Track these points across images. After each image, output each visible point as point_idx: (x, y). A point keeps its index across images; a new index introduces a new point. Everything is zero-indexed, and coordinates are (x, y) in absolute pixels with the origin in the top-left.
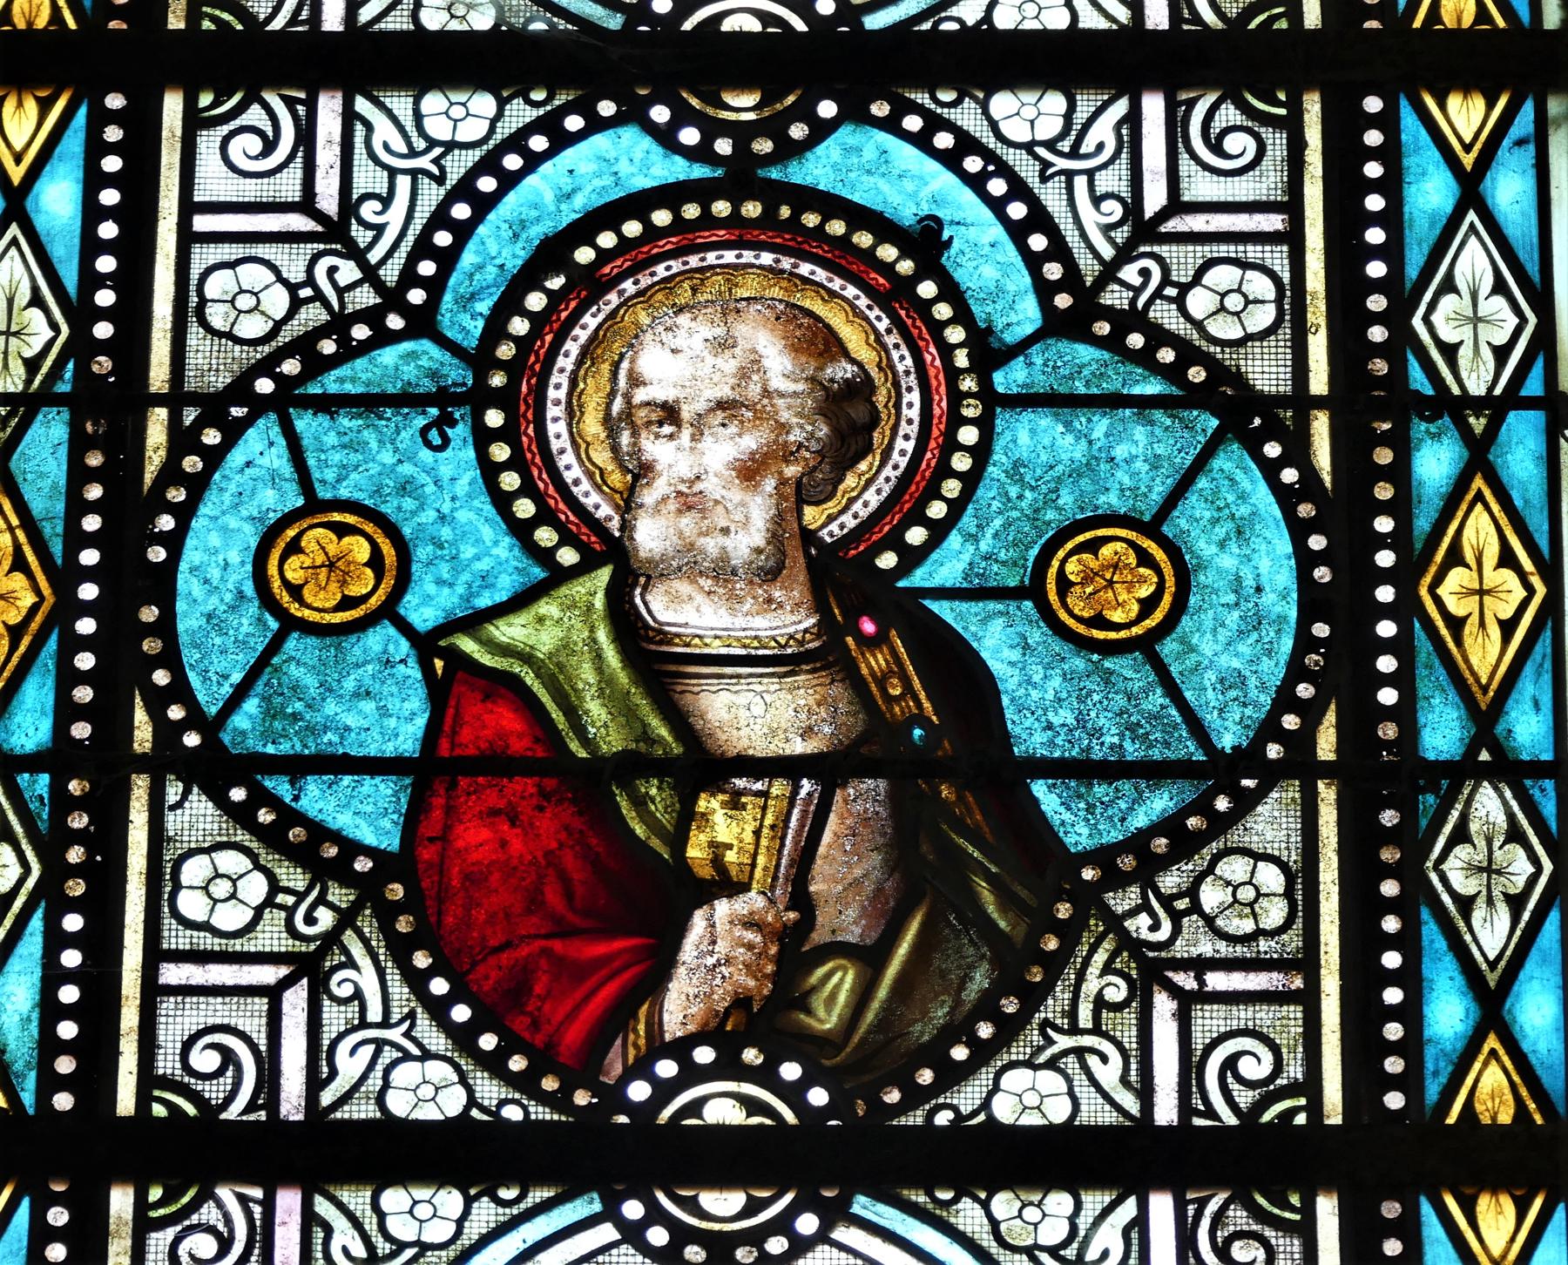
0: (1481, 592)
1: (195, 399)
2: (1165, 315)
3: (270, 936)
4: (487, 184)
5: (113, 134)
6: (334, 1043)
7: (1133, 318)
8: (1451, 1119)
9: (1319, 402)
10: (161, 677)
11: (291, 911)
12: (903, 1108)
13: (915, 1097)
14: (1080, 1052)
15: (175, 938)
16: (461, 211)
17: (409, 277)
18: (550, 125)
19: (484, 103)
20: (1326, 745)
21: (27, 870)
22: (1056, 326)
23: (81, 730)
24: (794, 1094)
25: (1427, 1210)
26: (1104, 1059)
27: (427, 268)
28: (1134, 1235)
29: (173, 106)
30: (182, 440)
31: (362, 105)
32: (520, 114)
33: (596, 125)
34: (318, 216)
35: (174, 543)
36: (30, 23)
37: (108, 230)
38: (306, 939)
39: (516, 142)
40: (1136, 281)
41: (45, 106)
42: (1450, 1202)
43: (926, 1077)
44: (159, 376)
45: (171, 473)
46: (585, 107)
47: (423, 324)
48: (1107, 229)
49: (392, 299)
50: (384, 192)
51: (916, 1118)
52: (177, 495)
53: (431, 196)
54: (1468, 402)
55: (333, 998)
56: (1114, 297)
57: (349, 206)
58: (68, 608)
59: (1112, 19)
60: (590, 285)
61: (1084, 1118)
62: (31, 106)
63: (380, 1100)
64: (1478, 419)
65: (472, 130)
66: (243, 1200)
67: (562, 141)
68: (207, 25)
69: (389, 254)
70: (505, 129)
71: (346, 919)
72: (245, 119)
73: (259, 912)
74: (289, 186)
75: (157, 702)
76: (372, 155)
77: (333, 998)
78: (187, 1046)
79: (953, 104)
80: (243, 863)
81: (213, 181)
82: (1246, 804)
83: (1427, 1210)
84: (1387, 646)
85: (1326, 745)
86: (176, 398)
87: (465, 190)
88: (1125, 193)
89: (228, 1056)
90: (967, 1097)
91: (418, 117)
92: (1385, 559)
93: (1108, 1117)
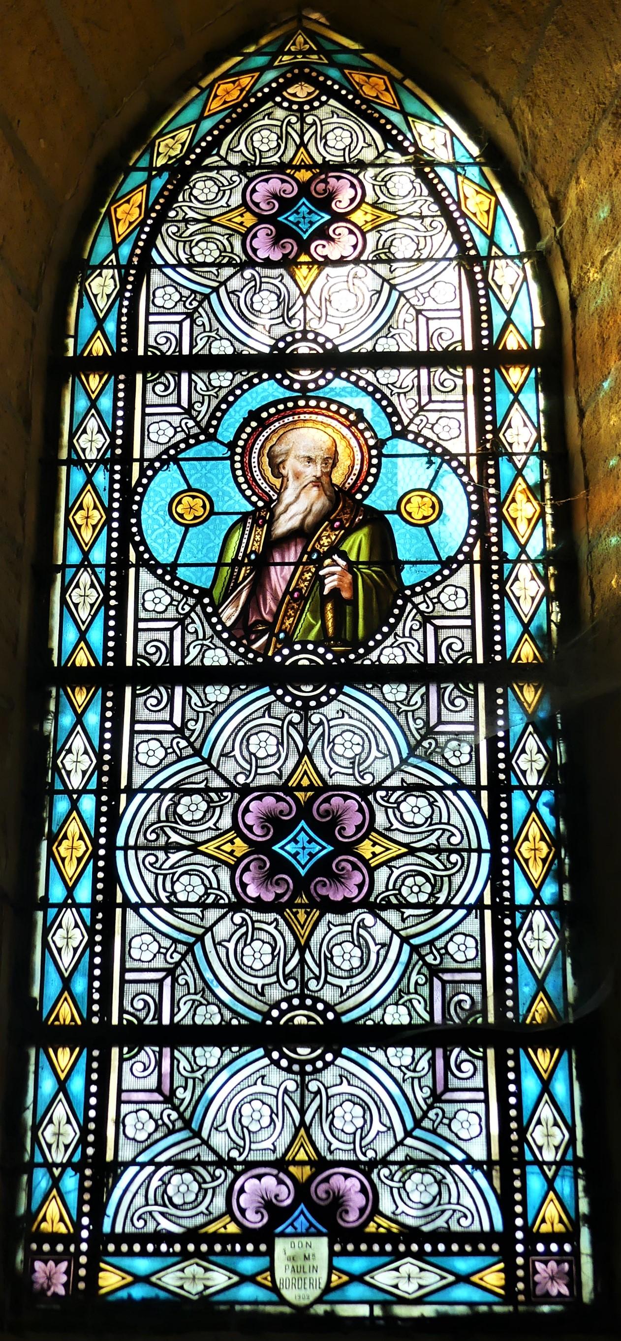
0: (535, 850)
1: (147, 460)
3: (159, 963)
4: (231, 399)
5: (121, 386)
6: (188, 646)
7: (418, 435)
8: (500, 348)
9: (484, 788)
10: (137, 538)
11: (177, 606)
12: (356, 659)
13: (359, 657)
14: (406, 643)
15: (142, 615)
16: (224, 406)
17: (209, 425)
19: (229, 375)
21: (99, 595)
22: (396, 435)
23: (100, 898)
25: (522, 1052)
26: (413, 645)
27: (214, 423)
28: (425, 698)
29: (139, 378)
31: (194, 377)
32: (239, 379)
33: (262, 381)
34: (182, 408)
35: (140, 504)
36: (81, 689)
37: (111, 654)
38: (181, 614)
39: (239, 386)
40: (427, 746)
41: (101, 378)
42: (530, 1050)
43: (361, 651)
44: (136, 455)
45: (139, 483)
46: (259, 376)
47: (212, 438)
49: (204, 431)
50: (195, 718)
51: (359, 662)
52: (140, 490)
53: (215, 403)
54: (529, 787)
55: (188, 632)
56: (412, 428)
57: (184, 723)
58: (109, 520)
59: (418, 660)
60: (263, 424)
61: (408, 662)
62: (97, 377)
63: (202, 661)
64: (559, 1293)
65: (226, 383)
66: (154, 1052)
67: (252, 385)
68: (150, 354)
69: (197, 738)
70: (235, 383)
71: (193, 608)
72: (153, 694)
74: (173, 399)
75: (136, 546)
76: (197, 392)
77: (188, 632)
79: (372, 688)
80: (162, 593)
81: (151, 398)
82: (453, 572)
83: (522, 1052)
84: (506, 867)
86: (142, 460)
87: (224, 400)
88: (424, 717)
89: (158, 648)
90: (374, 656)
91: (210, 380)
92: (495, 558)
93: (414, 662)
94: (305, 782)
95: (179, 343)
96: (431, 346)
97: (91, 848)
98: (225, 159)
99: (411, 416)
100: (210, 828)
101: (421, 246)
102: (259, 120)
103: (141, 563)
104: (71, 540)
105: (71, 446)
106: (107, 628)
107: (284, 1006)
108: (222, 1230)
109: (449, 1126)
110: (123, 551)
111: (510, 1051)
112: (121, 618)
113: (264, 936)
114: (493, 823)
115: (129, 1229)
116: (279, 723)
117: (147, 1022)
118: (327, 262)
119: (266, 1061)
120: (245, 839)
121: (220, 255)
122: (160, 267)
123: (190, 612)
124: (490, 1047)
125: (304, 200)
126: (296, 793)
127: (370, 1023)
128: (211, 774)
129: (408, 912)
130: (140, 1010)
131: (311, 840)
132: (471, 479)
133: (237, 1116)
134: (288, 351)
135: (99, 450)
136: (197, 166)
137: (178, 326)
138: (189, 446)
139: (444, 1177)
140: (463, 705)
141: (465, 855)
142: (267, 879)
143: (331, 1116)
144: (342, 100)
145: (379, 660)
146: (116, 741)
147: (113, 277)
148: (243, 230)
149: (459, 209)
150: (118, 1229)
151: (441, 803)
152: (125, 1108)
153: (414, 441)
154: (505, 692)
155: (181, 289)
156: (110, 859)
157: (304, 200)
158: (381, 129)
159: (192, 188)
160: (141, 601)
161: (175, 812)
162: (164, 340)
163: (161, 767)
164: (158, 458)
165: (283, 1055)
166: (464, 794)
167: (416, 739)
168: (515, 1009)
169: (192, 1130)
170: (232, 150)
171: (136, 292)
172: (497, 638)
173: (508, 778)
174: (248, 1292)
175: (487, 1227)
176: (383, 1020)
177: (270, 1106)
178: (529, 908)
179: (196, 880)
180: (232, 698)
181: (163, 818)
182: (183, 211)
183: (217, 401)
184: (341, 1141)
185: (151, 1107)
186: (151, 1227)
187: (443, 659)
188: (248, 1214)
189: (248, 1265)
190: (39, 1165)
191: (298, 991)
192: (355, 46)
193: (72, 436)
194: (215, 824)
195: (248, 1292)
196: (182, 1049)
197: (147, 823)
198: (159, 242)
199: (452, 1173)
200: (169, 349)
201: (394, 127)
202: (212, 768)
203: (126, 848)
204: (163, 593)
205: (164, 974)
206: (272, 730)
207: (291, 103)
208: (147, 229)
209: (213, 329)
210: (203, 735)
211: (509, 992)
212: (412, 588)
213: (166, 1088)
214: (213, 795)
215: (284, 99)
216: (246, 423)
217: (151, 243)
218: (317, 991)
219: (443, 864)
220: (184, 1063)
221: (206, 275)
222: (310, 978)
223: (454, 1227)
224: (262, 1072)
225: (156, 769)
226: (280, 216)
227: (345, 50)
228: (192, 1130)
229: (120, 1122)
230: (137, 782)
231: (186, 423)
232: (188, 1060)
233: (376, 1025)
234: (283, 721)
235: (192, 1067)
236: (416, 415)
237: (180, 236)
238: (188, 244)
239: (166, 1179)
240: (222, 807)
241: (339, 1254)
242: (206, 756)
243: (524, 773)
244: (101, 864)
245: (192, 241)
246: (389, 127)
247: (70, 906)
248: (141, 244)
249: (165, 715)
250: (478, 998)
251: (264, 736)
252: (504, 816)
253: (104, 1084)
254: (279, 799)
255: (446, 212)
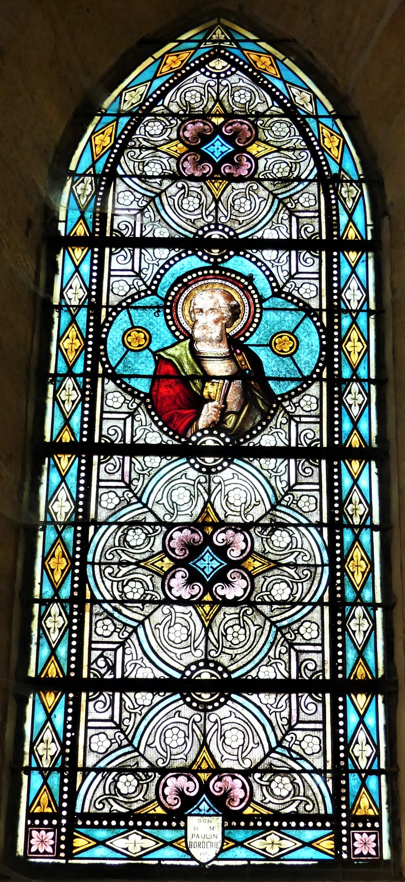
1: (111, 306)
2: (295, 293)
7: (289, 294)
13: (246, 440)
17: (152, 284)
18: (179, 255)
20: (324, 375)
22: (274, 295)
23: (89, 369)
24: (223, 440)
30: (108, 314)
32: (173, 253)
39: (173, 258)
42: (347, 461)
44: (104, 302)
46: (186, 252)
47: (154, 293)
48: (284, 277)
49: (149, 288)
51: (246, 445)
53: (156, 269)
56: (286, 290)
58: (86, 346)
60: (186, 286)
67: (181, 258)
68: (114, 235)
70: (170, 256)
73: (112, 633)
75: (103, 364)
78: (108, 429)
82: (309, 386)
85: (324, 375)
86: (107, 306)
87: (163, 267)
90: (256, 441)
94: (204, 766)
95: (134, 229)
96: (299, 442)
97: (73, 507)
98: (167, 108)
99: (285, 281)
100: (148, 551)
101: (293, 169)
102: (188, 83)
103: (105, 375)
104: (43, 641)
105: (47, 510)
106: (83, 416)
107: (206, 229)
108: (152, 812)
109: (297, 504)
110: (94, 367)
111: (341, 699)
112: (92, 410)
113: (195, 194)
114: (331, 549)
115: (93, 810)
116: (187, 721)
117: (116, 442)
118: (225, 602)
119: (188, 465)
120: (171, 558)
121: (144, 593)
122: (121, 177)
123: (147, 205)
124: (328, 692)
125: (217, 161)
126: (199, 774)
127: (250, 678)
128: (140, 758)
129: (275, 607)
130: (101, 668)
131: (222, 145)
132: (322, 324)
133: (163, 737)
134: (205, 237)
135: (80, 300)
136: (148, 112)
137: (123, 421)
138: (140, 298)
139: (294, 533)
140: (312, 262)
141: (313, 570)
142: (196, 165)
143: (223, 738)
144: (245, 72)
145: (257, 676)
146: (87, 492)
147: (91, 183)
148: (177, 155)
149: (319, 144)
150: (86, 810)
151: (297, 535)
152: (101, 491)
153: (285, 298)
154: (345, 700)
155: (135, 193)
156: (83, 568)
157: (217, 161)
158: (269, 91)
159: (145, 126)
160: (94, 627)
161: (125, 540)
162: (124, 227)
163: (107, 754)
164: (120, 305)
165: (197, 462)
166: (312, 529)
167: (281, 494)
168: (340, 439)
169: (142, 503)
170: (149, 746)
171: (106, 192)
172: (336, 429)
173: (341, 519)
174: (168, 853)
175: (322, 812)
176: (257, 676)
177: (184, 731)
178: (350, 381)
179: (139, 585)
180: (154, 702)
181: (107, 792)
182: (109, 803)
183: (158, 268)
184: (230, 754)
185: (107, 731)
186: (106, 810)
187: (302, 237)
188: (177, 552)
189: (168, 835)
190: (35, 769)
191: (203, 657)
192: (252, 37)
193: (48, 503)
194: (150, 548)
195: (168, 853)
196: (128, 694)
197: (106, 548)
198: (122, 160)
199: (299, 531)
200: (127, 233)
201: (278, 90)
202: (141, 755)
203: (93, 564)
204: (120, 395)
205: (127, 415)
206: (188, 487)
207: (212, 73)
208: (115, 151)
209: (139, 658)
210: (134, 730)
211: (335, 272)
212: (282, 395)
213: (127, 479)
214: (141, 774)
215: (207, 70)
216: (175, 284)
217: (117, 162)
218: (216, 657)
219: (299, 575)
220: (138, 466)
221: (135, 609)
222: (212, 650)
223: (301, 810)
224: (184, 472)
225: (113, 490)
226: (203, 146)
227: (248, 40)
228: (142, 503)
229: (98, 502)
230: (90, 763)
231: (119, 736)
232: (140, 463)
233: (253, 679)
234: (189, 720)
235: (143, 468)
236: (288, 281)
237: (137, 159)
238: (120, 583)
239: (116, 778)
240: (171, 128)
241: (227, 828)
242: (136, 746)
243: (349, 301)
244: (87, 406)
245: (123, 581)
246: (274, 90)
247: (56, 601)
248: (111, 160)
249: (129, 266)
250: (319, 663)
251: (175, 730)
252: (336, 327)
253: (88, 478)
254: (193, 532)
255: (310, 146)
